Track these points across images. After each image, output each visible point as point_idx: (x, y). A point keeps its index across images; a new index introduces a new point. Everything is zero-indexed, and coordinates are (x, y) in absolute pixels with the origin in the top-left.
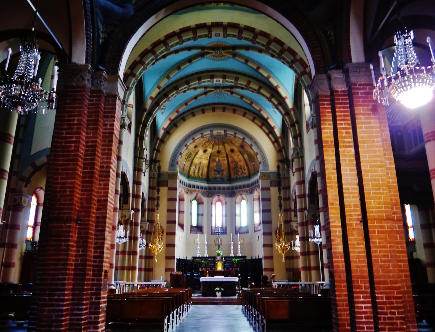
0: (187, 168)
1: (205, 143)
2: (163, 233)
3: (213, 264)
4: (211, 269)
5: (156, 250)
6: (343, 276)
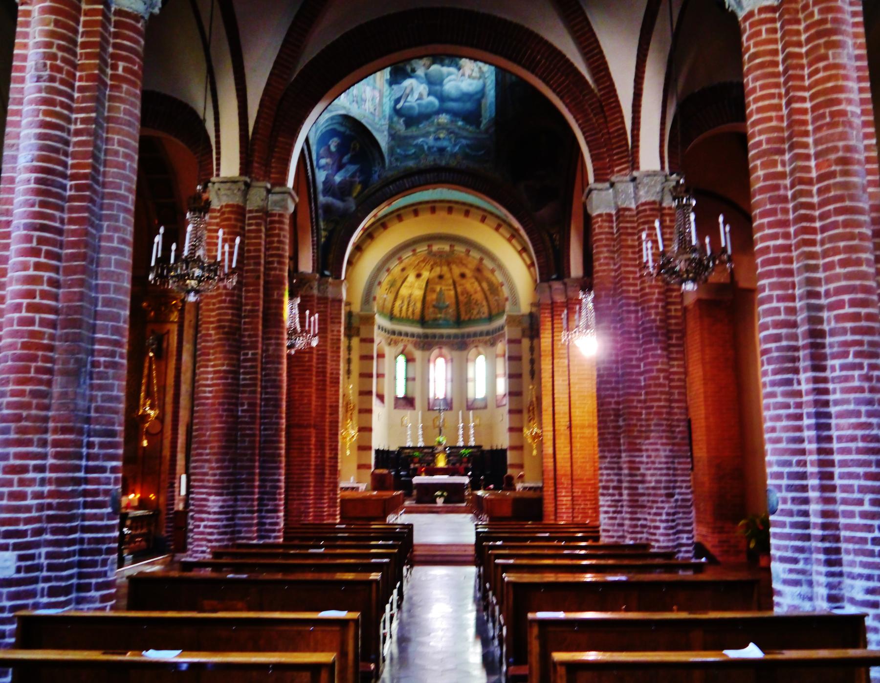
0: (389, 305)
4: (429, 464)
6: (551, 474)
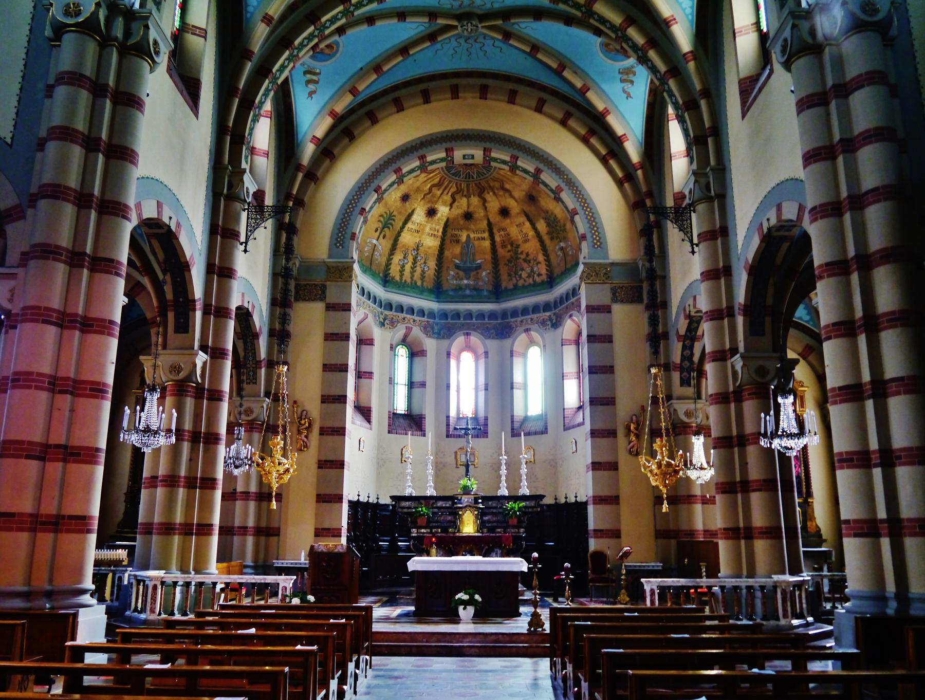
0: (380, 257)
1: (430, 190)
2: (309, 428)
3: (449, 518)
4: (445, 530)
5: (275, 474)
